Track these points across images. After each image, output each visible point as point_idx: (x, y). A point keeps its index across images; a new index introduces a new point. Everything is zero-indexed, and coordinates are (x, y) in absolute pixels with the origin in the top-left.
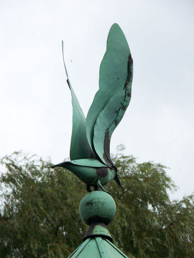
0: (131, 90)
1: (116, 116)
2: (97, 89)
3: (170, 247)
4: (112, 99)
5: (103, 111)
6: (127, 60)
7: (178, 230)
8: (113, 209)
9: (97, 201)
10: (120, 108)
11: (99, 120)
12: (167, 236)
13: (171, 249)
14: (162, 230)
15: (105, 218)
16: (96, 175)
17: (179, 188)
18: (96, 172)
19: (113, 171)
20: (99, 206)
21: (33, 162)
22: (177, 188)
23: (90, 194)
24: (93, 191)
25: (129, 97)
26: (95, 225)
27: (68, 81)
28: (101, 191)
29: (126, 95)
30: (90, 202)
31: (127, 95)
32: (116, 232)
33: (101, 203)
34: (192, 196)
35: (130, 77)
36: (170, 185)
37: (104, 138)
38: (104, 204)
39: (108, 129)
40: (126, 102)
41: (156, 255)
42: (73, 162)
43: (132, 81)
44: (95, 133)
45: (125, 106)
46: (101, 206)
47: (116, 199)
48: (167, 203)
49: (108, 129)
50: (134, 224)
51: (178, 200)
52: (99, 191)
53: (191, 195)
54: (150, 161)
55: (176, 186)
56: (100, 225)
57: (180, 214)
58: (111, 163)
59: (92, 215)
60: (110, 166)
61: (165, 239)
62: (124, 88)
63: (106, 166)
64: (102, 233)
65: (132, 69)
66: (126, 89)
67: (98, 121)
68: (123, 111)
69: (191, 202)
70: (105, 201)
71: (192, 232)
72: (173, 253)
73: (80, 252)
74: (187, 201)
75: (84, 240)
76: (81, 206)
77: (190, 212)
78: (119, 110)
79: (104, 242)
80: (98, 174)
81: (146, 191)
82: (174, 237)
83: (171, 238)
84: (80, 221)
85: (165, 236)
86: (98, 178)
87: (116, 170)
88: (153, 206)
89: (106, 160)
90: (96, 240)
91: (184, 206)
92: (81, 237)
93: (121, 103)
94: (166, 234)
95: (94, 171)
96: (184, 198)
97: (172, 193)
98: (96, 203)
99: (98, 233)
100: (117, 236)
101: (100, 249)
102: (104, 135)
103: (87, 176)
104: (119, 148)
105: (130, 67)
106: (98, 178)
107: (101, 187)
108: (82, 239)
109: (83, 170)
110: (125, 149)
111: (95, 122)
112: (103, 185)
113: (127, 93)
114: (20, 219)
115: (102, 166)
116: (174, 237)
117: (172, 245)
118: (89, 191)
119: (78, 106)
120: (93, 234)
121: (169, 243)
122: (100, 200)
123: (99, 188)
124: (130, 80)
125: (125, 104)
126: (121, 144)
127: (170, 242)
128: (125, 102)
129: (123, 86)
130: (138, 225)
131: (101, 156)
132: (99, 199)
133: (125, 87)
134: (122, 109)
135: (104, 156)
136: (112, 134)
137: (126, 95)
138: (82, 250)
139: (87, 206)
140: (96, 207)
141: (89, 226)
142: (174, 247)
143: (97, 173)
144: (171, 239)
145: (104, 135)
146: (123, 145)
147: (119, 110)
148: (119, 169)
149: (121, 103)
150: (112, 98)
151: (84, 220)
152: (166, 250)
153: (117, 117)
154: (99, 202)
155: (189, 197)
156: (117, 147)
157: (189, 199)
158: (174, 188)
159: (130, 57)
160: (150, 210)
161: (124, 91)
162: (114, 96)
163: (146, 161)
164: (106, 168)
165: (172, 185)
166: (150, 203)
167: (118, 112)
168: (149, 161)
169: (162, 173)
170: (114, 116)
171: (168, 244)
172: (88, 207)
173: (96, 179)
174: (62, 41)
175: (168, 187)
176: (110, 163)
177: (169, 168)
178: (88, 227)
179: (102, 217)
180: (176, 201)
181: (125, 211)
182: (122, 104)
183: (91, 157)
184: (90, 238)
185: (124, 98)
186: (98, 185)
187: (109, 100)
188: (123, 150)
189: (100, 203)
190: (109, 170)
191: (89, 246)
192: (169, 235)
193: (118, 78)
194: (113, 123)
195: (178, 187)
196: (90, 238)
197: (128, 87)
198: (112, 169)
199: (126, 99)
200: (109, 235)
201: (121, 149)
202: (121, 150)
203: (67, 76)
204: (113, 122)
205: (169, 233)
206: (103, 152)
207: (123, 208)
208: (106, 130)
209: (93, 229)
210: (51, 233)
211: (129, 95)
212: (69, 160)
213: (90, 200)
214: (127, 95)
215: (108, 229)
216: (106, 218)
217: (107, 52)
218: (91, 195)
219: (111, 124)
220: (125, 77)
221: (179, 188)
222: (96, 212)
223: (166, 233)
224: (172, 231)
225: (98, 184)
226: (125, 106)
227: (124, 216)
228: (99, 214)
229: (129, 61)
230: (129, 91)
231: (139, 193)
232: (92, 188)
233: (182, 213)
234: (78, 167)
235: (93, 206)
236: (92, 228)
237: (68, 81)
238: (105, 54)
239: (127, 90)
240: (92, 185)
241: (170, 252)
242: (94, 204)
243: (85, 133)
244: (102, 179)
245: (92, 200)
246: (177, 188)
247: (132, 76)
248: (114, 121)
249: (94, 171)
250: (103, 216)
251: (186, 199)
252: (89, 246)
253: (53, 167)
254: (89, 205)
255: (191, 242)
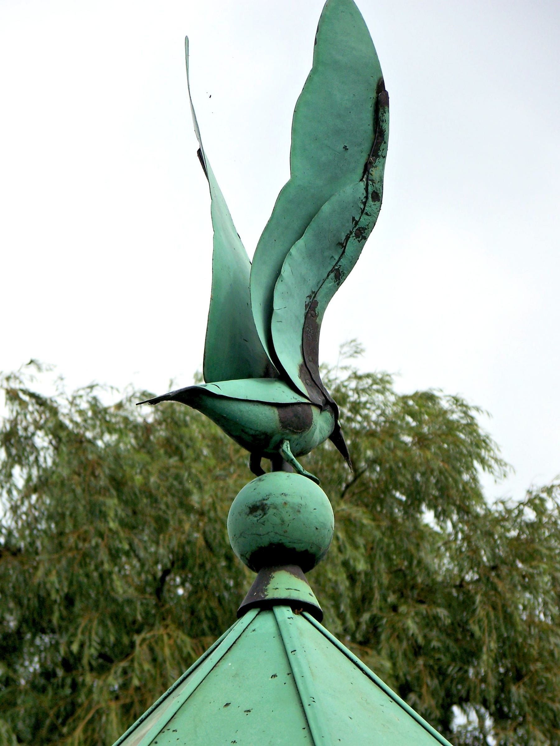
0: (381, 181)
1: (337, 258)
2: (286, 177)
3: (487, 634)
4: (326, 208)
5: (301, 243)
6: (374, 95)
7: (515, 586)
8: (324, 525)
9: (279, 501)
10: (351, 233)
11: (289, 268)
12: (481, 602)
13: (489, 642)
14: (464, 584)
15: (303, 549)
16: (279, 425)
17: (514, 472)
18: (277, 417)
19: (328, 415)
20: (287, 518)
21: (217, 578)
22: (507, 469)
23: (260, 480)
24: (269, 471)
25: (377, 203)
26: (274, 571)
27: (200, 154)
28: (291, 472)
29: (367, 197)
30: (258, 504)
31: (370, 196)
32: (334, 589)
33: (292, 508)
34: (552, 487)
35: (381, 143)
36: (490, 459)
37: (302, 321)
38: (299, 511)
39: (313, 292)
40: (366, 217)
41: (442, 656)
42: (211, 387)
43: (384, 157)
44: (277, 305)
45: (364, 229)
46: (291, 517)
47: (333, 494)
48: (480, 510)
49: (315, 293)
50: (383, 566)
51: (510, 499)
52: (287, 471)
53: (549, 485)
54: (434, 389)
55: (506, 464)
56: (287, 571)
57: (518, 538)
58: (323, 393)
59: (265, 542)
60: (320, 400)
61: (474, 611)
62: (362, 175)
63: (306, 401)
64: (295, 595)
65: (387, 121)
66: (367, 179)
67: (286, 270)
68: (359, 241)
69: (550, 505)
70: (303, 502)
71: (552, 593)
72: (493, 655)
73: (229, 649)
74: (537, 502)
75: (242, 613)
76: (233, 514)
77: (547, 534)
78: (347, 238)
79: (299, 620)
80: (285, 424)
81: (423, 474)
82: (500, 607)
83: (490, 609)
84: (229, 558)
85: (474, 603)
86: (283, 434)
87: (336, 415)
88: (437, 516)
89: (306, 384)
90: (274, 614)
91: (530, 515)
92: (233, 607)
93: (354, 219)
94: (478, 598)
95: (273, 414)
96: (529, 492)
97: (496, 481)
98: (275, 508)
99: (283, 594)
100: (335, 598)
101: (286, 641)
102: (303, 312)
103: (251, 429)
104: (346, 349)
105: (380, 115)
106: (284, 436)
107: (292, 460)
108: (235, 610)
109: (241, 411)
110: (363, 354)
111: (277, 274)
112: (297, 455)
113: (370, 189)
114: (59, 561)
115: (294, 401)
116: (500, 607)
117: (494, 631)
118: (257, 471)
119: (202, 153)
120: (267, 597)
121: (486, 622)
122: (288, 499)
123: (287, 465)
124: (380, 153)
125: (364, 221)
126: (353, 338)
127: (489, 622)
128: (364, 216)
129: (360, 170)
130: (397, 572)
131: (293, 371)
132: (285, 495)
133: (364, 173)
134: (357, 236)
135: (301, 371)
136: (324, 309)
137: (367, 197)
138: (234, 643)
139: (251, 517)
140: (277, 520)
141: (255, 575)
142: (500, 636)
143: (281, 421)
144: (492, 614)
145: (301, 312)
146: (358, 342)
147: (347, 238)
148: (345, 411)
149: (354, 219)
150: (326, 203)
151: (242, 555)
152: (477, 645)
153: (340, 258)
154: (285, 503)
155: (542, 492)
156: (342, 346)
157: (544, 495)
158: (499, 468)
159: (381, 87)
160: (427, 525)
161: (362, 185)
162: (334, 199)
163: (423, 388)
164: (306, 407)
165: (496, 460)
166: (429, 507)
167: (342, 245)
168: (430, 389)
169: (468, 425)
170: (332, 257)
171: (480, 628)
172: (252, 519)
173: (276, 438)
174: (187, 39)
175: (483, 461)
176: (318, 393)
177: (488, 414)
178: (252, 576)
179: (294, 549)
180: (503, 502)
181: (363, 525)
182: (357, 223)
183: (262, 374)
184: (259, 610)
185: (362, 206)
186: (282, 454)
187: (318, 209)
188: (359, 355)
189: (287, 508)
190: (315, 411)
191: (254, 630)
192: (485, 599)
193: (345, 148)
194: (330, 277)
195: (511, 466)
196: (259, 610)
197: (374, 172)
198: (324, 410)
199: (367, 209)
200: (313, 600)
201: (352, 352)
202: (351, 356)
203: (199, 139)
204: (328, 275)
205: (485, 594)
206: (300, 360)
207: (355, 518)
208: (310, 297)
209: (268, 583)
210: (141, 590)
211: (377, 197)
212: (202, 384)
213: (260, 498)
214: (370, 196)
215: (308, 582)
216: (306, 551)
217: (314, 71)
218: (261, 483)
219: (324, 281)
220: (367, 146)
221: (514, 472)
222: (276, 533)
223: (476, 593)
224: (495, 589)
225: (283, 451)
226: (364, 229)
227: (360, 541)
228: (285, 541)
229: (377, 98)
230: (377, 186)
231: (404, 478)
232: (265, 463)
233: (523, 537)
234: (225, 404)
235: (267, 515)
236: (264, 581)
237: (200, 154)
238: (310, 79)
239: (370, 182)
240: (267, 456)
241: (485, 649)
242: (271, 512)
243: (249, 305)
244: (295, 436)
245: (264, 500)
246: (507, 469)
247: (386, 143)
248: (332, 271)
249: (273, 414)
250: (296, 546)
251: (537, 497)
252: (254, 630)
253: (154, 401)
254: (256, 511)
255: (549, 621)
